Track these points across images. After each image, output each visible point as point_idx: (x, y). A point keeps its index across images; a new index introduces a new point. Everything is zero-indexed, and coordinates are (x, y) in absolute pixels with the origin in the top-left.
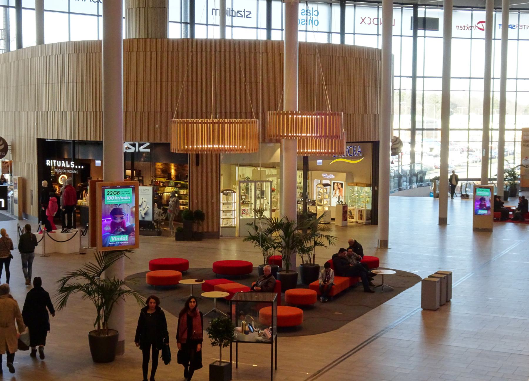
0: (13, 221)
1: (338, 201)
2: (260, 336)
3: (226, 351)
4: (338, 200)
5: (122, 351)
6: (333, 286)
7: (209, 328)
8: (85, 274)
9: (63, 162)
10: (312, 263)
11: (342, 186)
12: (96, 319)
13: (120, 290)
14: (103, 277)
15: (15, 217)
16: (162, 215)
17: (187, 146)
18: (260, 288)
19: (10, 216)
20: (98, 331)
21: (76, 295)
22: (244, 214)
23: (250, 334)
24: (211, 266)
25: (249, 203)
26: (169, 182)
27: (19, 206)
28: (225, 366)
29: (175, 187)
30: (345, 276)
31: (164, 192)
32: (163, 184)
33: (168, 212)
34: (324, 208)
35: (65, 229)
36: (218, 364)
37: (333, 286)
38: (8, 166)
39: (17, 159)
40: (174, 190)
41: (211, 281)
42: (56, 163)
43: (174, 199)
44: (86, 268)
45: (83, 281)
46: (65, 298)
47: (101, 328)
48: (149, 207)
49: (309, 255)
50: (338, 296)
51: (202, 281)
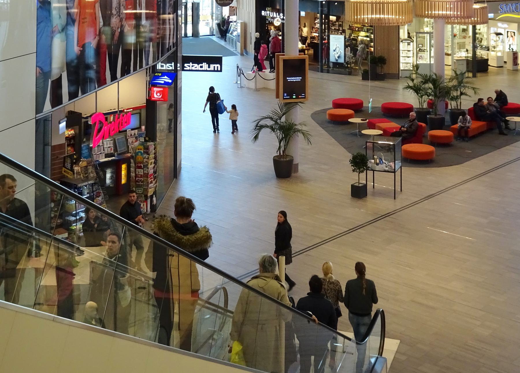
0: (236, 56)
1: (509, 49)
2: (386, 167)
3: (363, 175)
4: (509, 48)
5: (296, 170)
6: (469, 129)
7: (351, 160)
8: (271, 119)
9: (275, 13)
10: (459, 108)
11: (514, 35)
12: (278, 148)
13: (295, 129)
14: (283, 119)
15: (238, 52)
16: (352, 58)
17: (360, 16)
18: (406, 129)
19: (234, 52)
20: (280, 156)
21: (265, 132)
22: (421, 60)
23: (380, 165)
24: (380, 106)
25: (425, 50)
26: (363, 27)
27: (241, 44)
28: (362, 186)
29: (368, 32)
30: (484, 121)
31: (359, 36)
32: (358, 29)
33: (357, 56)
34: (496, 54)
35: (272, 70)
36: (357, 185)
37: (469, 129)
38: (234, 10)
39: (241, 7)
40: (367, 35)
41: (374, 120)
42: (269, 14)
43: (362, 45)
44: (271, 112)
45: (270, 123)
46: (258, 133)
47: (282, 154)
48: (342, 52)
49: (457, 102)
50: (474, 137)
51: (366, 120)
